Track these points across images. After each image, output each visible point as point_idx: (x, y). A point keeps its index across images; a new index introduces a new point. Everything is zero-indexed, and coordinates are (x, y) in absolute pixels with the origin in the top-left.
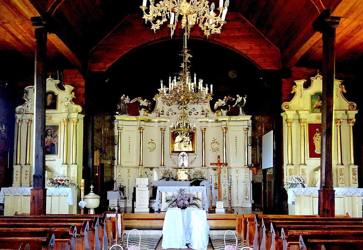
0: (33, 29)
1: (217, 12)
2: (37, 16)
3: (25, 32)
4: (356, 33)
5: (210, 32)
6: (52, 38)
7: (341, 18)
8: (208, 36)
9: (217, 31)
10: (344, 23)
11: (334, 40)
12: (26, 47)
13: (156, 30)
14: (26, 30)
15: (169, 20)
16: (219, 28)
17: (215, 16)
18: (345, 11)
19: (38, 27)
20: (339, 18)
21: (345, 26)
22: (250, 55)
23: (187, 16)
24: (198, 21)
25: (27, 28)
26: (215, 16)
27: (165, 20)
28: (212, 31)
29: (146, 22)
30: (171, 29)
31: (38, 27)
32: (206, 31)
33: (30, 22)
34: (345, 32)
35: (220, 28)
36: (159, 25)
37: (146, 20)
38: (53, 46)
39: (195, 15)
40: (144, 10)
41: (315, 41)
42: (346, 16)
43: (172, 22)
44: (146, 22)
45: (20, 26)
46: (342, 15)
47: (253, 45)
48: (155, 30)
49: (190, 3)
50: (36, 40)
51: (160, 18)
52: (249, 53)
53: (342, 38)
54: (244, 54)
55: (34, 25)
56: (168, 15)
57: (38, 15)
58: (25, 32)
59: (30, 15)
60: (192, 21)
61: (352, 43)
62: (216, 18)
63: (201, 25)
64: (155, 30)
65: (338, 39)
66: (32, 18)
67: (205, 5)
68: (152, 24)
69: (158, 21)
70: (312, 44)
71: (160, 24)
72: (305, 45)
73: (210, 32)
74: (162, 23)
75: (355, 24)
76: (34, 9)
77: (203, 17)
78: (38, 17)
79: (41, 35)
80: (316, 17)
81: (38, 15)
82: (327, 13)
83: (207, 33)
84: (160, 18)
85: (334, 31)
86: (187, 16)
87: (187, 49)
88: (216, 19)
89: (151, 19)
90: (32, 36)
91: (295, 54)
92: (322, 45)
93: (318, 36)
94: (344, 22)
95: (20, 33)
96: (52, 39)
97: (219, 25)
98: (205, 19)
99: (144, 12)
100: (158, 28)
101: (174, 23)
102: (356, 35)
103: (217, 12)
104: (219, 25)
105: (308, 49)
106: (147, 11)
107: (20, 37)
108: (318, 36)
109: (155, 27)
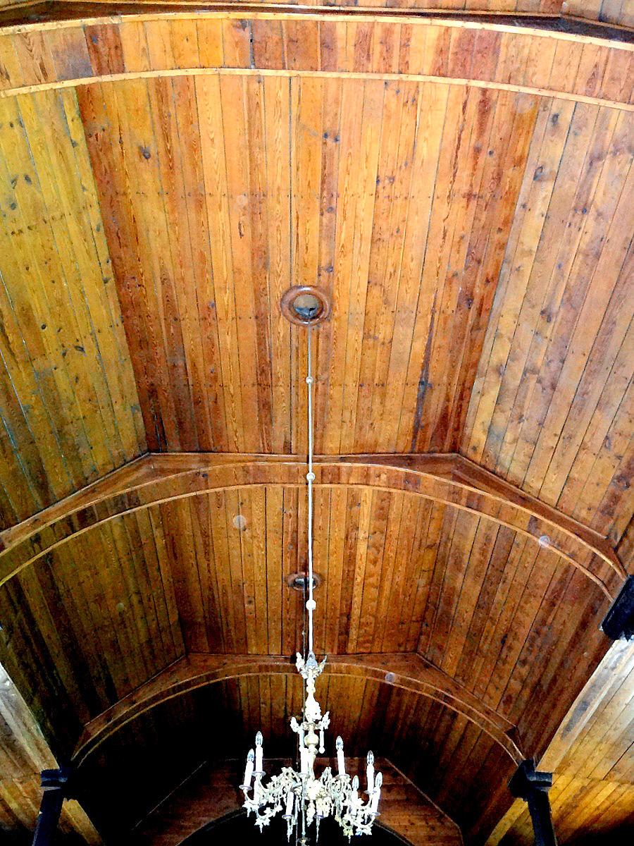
0: (41, 791)
1: (366, 799)
2: (54, 768)
3: (26, 795)
4: (581, 799)
5: (355, 832)
6: (71, 808)
7: (553, 775)
8: (350, 838)
9: (365, 831)
10: (558, 782)
11: (549, 815)
12: (19, 823)
13: (265, 827)
14: (27, 793)
15: (284, 807)
16: (369, 824)
17: (362, 805)
18: (556, 763)
19: (49, 788)
20: (549, 775)
21: (561, 788)
22: (410, 837)
23: (314, 802)
24: (332, 810)
25: (29, 789)
26: (362, 805)
27: (279, 808)
28: (357, 830)
29: (261, 830)
30: (288, 823)
31: (49, 788)
32: (346, 827)
33: (38, 777)
34: (563, 798)
35: (370, 824)
36: (265, 814)
37: (249, 811)
38: (67, 823)
39: (328, 800)
40: (245, 792)
41: (517, 815)
42: (560, 771)
43: (289, 811)
44: (261, 830)
45: (19, 785)
46: (553, 770)
47: (413, 818)
48: (261, 827)
49: (321, 780)
50: (40, 813)
51: (271, 806)
52: (408, 832)
53: (560, 807)
54: (400, 836)
55: (44, 784)
56: (285, 800)
57: (56, 766)
58: (26, 795)
59: (41, 767)
60: (324, 810)
61: (580, 818)
62: (363, 807)
63: (337, 818)
64: (261, 827)
65: (555, 809)
66: (43, 772)
67: (346, 785)
68: (258, 815)
69: (268, 810)
70: (514, 819)
71: (270, 816)
72: (502, 821)
73: (355, 832)
74: (274, 814)
75: (577, 784)
76: (51, 757)
77: (342, 805)
78: (56, 770)
79: (51, 804)
80: (512, 773)
81: (56, 766)
82: (529, 766)
83: (348, 832)
84: (271, 806)
85: (545, 796)
86: (314, 802)
87: (306, 836)
88: (363, 810)
89: (256, 808)
90: (35, 803)
91: (487, 838)
92: (530, 820)
93: (520, 807)
94: (559, 782)
95: (15, 798)
96: (70, 810)
97: (369, 819)
98: (345, 808)
99: (246, 795)
100: (267, 822)
101: (293, 812)
102: (583, 804)
103: (366, 799)
104: (369, 819)
105: (507, 828)
106: (251, 794)
107: (13, 805)
108: (520, 807)
109: (262, 821)
